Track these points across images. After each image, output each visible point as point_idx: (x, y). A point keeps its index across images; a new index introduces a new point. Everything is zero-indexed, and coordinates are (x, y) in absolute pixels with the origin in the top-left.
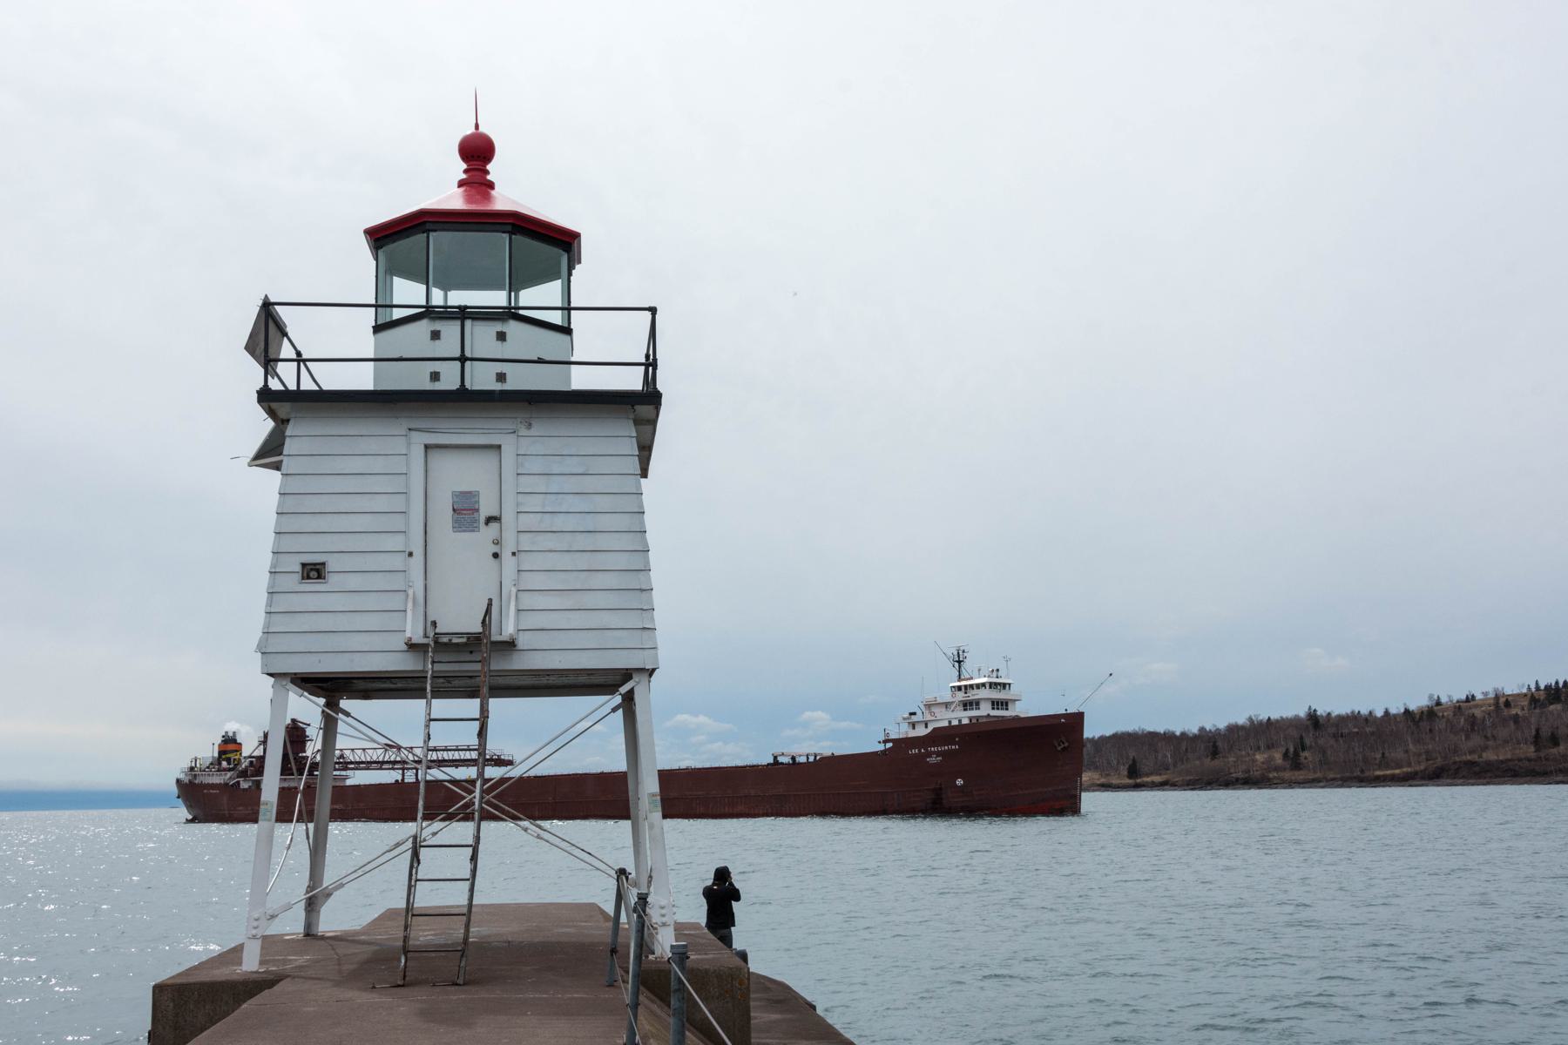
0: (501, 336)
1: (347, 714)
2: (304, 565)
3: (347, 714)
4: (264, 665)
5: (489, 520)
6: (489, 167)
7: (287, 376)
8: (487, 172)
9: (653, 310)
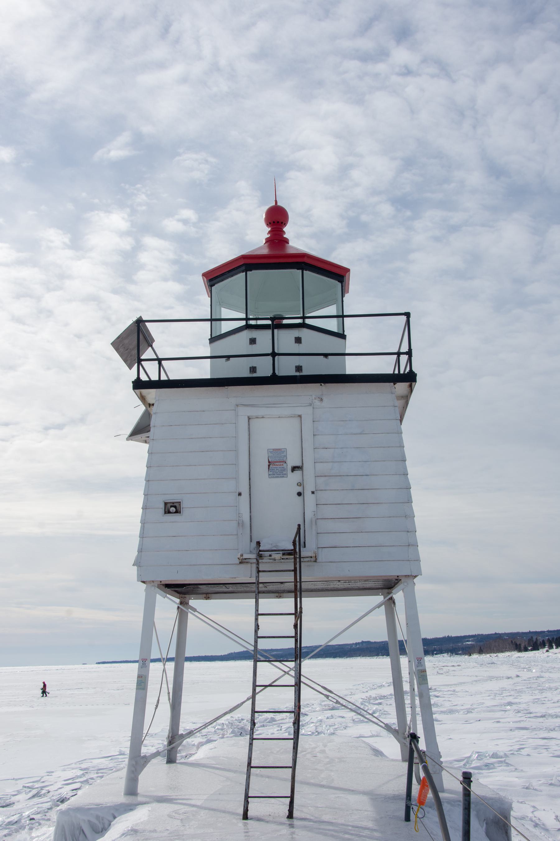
3: (195, 610)
4: (139, 575)
5: (294, 469)
7: (151, 372)
8: (284, 232)
9: (408, 315)
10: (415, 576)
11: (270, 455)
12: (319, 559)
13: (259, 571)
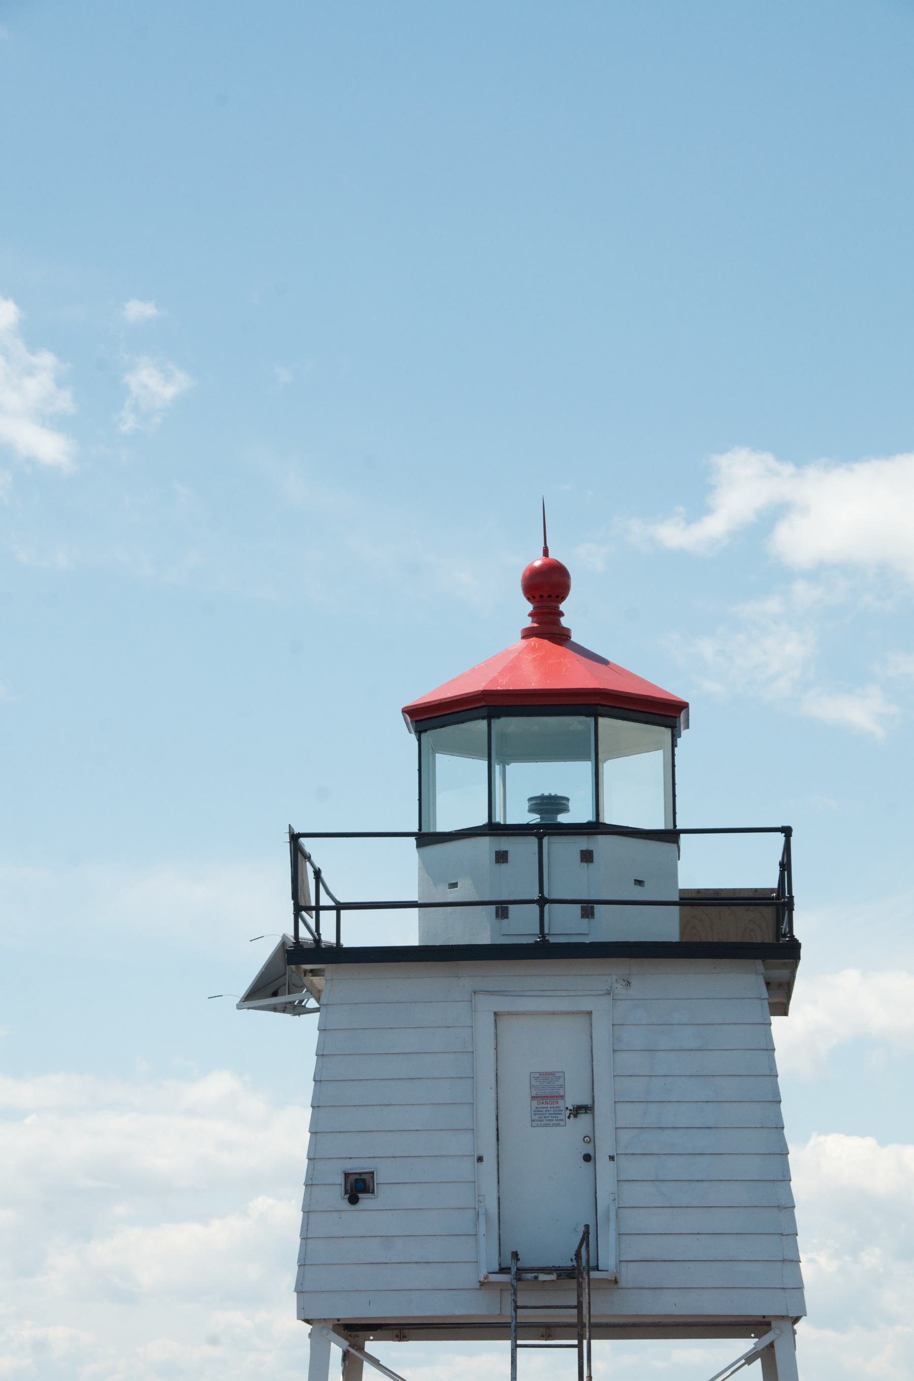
0: (587, 856)
1: (375, 1362)
2: (347, 1175)
3: (375, 1362)
5: (578, 1110)
6: (563, 607)
9: (787, 831)
10: (796, 1320)
11: (534, 1083)
12: (623, 1283)
13: (517, 1308)
